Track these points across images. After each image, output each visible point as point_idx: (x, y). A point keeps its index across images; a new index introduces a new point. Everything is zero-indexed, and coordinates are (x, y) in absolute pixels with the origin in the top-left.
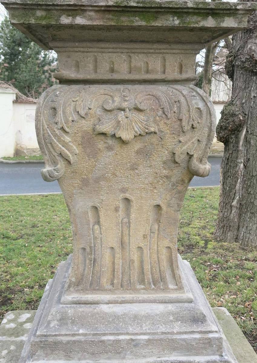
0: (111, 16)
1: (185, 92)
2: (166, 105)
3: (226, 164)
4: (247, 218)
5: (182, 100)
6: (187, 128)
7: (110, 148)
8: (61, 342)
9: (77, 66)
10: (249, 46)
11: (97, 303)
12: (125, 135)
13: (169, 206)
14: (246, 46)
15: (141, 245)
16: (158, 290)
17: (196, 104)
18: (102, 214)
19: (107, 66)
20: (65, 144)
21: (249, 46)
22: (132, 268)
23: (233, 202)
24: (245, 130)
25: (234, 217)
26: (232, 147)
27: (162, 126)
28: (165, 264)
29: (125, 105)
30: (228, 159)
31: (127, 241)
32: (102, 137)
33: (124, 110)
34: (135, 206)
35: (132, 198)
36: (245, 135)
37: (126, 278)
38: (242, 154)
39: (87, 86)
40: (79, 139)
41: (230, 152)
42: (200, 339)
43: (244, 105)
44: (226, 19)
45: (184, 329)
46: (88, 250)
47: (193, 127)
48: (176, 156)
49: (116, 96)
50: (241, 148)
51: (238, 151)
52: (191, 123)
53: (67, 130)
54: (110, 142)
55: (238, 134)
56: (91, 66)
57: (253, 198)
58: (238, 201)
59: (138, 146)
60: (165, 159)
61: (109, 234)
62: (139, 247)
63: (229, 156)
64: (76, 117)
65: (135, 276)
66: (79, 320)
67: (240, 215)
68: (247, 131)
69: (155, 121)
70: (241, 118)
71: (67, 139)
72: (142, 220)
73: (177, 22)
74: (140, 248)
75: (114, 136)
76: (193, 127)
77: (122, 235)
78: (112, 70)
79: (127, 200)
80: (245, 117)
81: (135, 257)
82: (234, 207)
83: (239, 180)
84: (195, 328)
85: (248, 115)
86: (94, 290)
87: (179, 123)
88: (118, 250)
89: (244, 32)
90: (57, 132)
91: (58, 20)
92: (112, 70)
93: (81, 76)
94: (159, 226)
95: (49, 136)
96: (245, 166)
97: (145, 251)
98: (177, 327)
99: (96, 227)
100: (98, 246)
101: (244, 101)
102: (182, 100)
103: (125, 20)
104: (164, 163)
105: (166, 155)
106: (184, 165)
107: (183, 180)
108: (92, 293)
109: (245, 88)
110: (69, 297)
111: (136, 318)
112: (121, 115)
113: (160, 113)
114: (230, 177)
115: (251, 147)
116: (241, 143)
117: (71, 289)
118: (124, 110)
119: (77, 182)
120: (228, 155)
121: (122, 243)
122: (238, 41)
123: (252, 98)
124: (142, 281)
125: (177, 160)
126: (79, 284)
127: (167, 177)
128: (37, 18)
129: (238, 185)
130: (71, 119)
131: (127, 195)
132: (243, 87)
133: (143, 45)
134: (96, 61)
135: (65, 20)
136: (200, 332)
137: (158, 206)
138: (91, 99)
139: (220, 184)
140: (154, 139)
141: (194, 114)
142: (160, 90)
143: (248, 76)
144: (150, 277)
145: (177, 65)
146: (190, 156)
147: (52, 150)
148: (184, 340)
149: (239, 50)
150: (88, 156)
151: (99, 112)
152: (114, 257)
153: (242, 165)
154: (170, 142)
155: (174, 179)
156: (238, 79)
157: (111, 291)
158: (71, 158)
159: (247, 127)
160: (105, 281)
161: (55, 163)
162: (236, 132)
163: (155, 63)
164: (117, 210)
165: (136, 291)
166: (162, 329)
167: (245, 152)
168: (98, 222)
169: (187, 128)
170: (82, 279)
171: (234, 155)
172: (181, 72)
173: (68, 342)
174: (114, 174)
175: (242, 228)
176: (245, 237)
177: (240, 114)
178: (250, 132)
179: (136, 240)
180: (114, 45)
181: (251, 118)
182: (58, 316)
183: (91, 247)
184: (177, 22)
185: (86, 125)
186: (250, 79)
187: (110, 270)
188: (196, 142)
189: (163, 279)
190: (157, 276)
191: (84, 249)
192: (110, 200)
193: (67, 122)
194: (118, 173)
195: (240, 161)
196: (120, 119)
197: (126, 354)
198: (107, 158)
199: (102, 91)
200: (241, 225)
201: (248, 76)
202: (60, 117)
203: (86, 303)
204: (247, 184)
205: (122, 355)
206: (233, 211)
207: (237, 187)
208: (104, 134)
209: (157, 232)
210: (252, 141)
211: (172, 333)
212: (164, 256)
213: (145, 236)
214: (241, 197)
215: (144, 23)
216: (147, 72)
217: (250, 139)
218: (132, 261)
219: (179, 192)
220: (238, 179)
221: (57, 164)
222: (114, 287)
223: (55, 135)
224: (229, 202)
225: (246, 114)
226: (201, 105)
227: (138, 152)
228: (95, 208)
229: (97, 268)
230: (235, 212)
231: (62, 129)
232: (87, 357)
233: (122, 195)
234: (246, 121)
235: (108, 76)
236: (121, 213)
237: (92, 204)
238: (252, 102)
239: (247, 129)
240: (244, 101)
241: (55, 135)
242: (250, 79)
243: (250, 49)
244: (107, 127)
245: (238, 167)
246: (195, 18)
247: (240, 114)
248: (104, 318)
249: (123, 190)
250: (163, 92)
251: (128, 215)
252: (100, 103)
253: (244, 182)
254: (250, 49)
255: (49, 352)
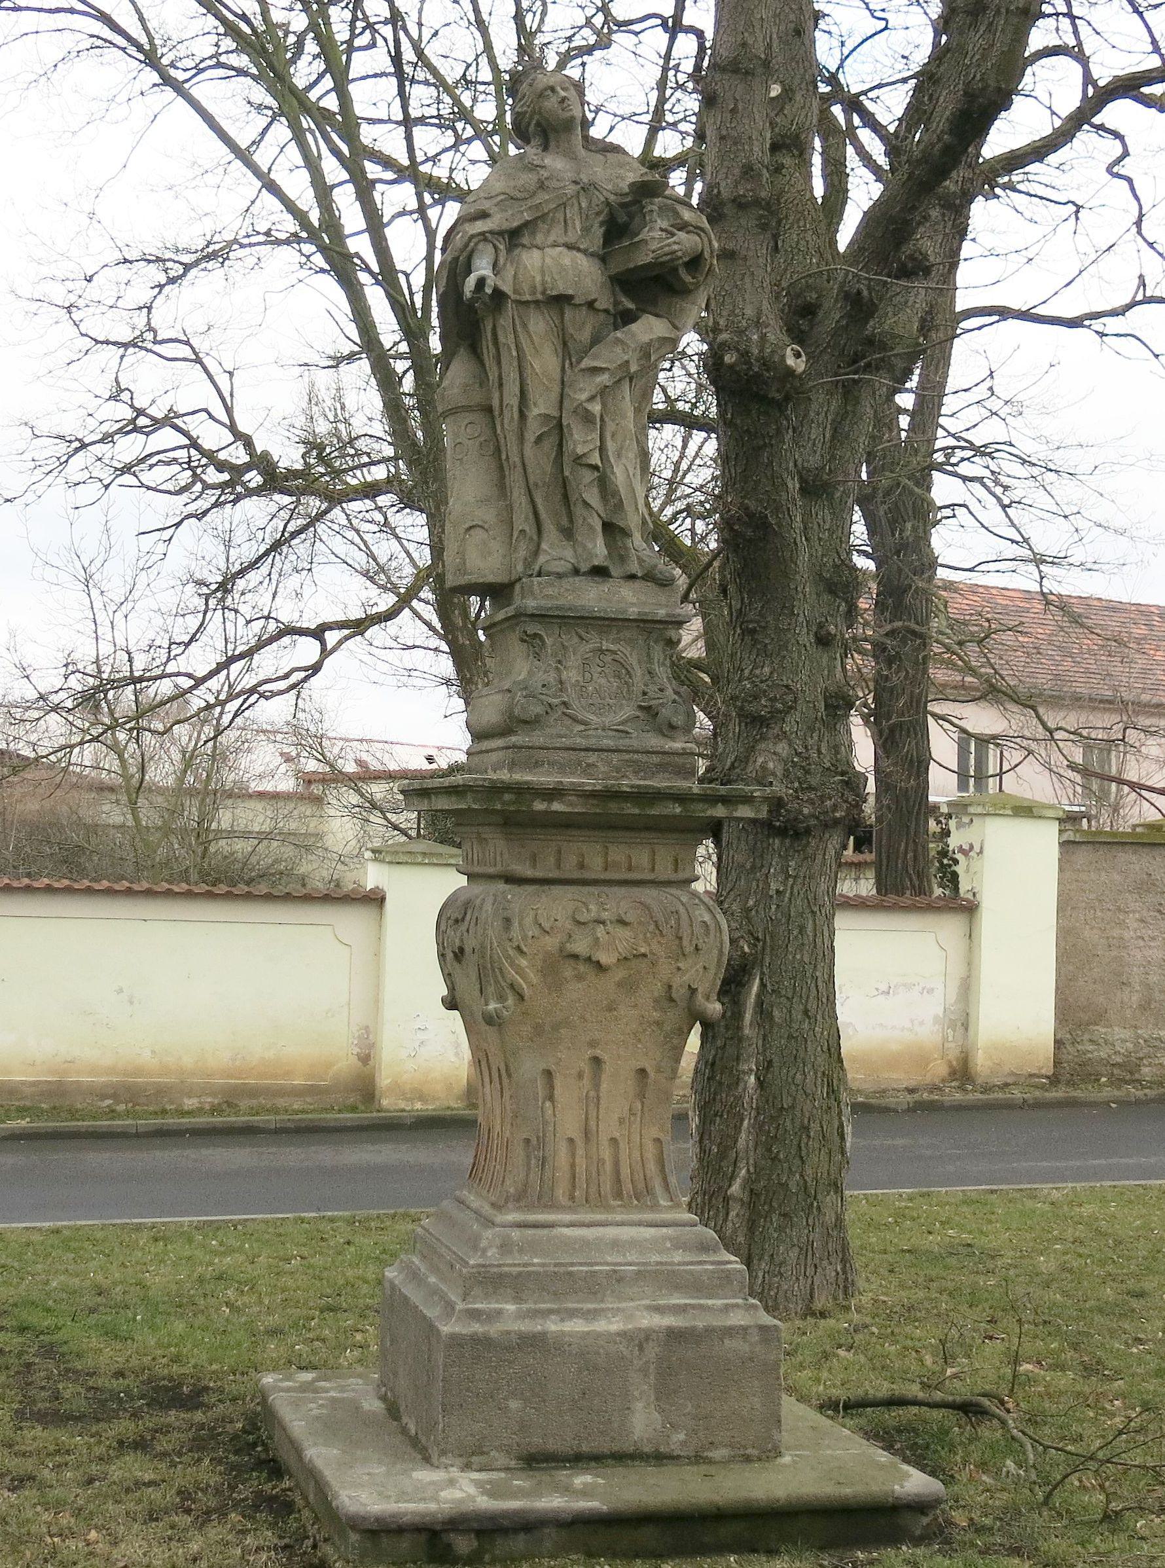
0: (595, 802)
1: (684, 899)
2: (660, 918)
3: (709, 1079)
4: (771, 1230)
5: (682, 910)
6: (689, 949)
7: (580, 978)
8: (508, 1275)
9: (534, 859)
10: (760, 760)
11: (551, 1226)
12: (605, 958)
13: (659, 1070)
14: (753, 759)
15: (617, 1135)
16: (642, 1208)
17: (700, 915)
18: (558, 1083)
19: (573, 860)
20: (520, 971)
21: (760, 760)
22: (602, 1173)
23: (730, 1186)
24: (757, 981)
25: (735, 1231)
26: (722, 1030)
27: (655, 947)
28: (652, 1167)
29: (605, 915)
30: (713, 1064)
31: (594, 1128)
32: (572, 962)
33: (603, 923)
34: (608, 1068)
35: (605, 1057)
36: (758, 996)
37: (593, 1190)
38: (751, 1049)
39: (546, 887)
40: (539, 963)
41: (719, 1043)
42: (713, 1272)
43: (753, 912)
44: (740, 806)
45: (688, 1259)
46: (534, 1141)
47: (697, 949)
48: (674, 991)
49: (593, 904)
50: (747, 1031)
51: (740, 1040)
52: (694, 943)
53: (525, 949)
54: (582, 968)
55: (739, 993)
56: (552, 860)
57: (786, 1171)
58: (747, 1181)
59: (619, 974)
60: (656, 994)
61: (568, 1120)
62: (612, 1139)
63: (715, 1057)
64: (537, 932)
65: (607, 1187)
66: (532, 1247)
67: (752, 1226)
68: (763, 985)
69: (646, 940)
70: (746, 949)
71: (524, 962)
72: (617, 1091)
73: (678, 810)
74: (614, 1141)
75: (589, 959)
76: (697, 949)
77: (587, 1119)
78: (581, 866)
79: (596, 1061)
80: (756, 946)
81: (606, 1153)
82: (735, 1199)
83: (746, 1122)
84: (704, 1258)
85: (765, 942)
86: (545, 1206)
87: (677, 942)
88: (580, 1143)
89: (746, 724)
90: (511, 952)
91: (530, 806)
92: (581, 866)
93: (539, 874)
94: (643, 1103)
95: (499, 957)
96: (761, 1083)
97: (621, 1145)
98: (678, 1256)
99: (548, 1104)
100: (550, 1135)
101: (751, 903)
102: (682, 910)
103: (613, 807)
104: (656, 1001)
105: (658, 989)
106: (684, 1004)
107: (680, 1029)
108: (542, 1212)
109: (753, 867)
110: (511, 1217)
111: (615, 1244)
112: (600, 931)
113: (652, 927)
114: (722, 1116)
115: (776, 1029)
116: (748, 1017)
117: (510, 1205)
118: (603, 923)
119: (526, 1029)
120: (713, 1052)
121: (587, 1133)
122: (731, 743)
123: (771, 897)
124: (618, 1195)
125: (674, 995)
126: (521, 1198)
127: (657, 1023)
128: (503, 804)
129: (743, 1135)
130: (530, 934)
131: (598, 1052)
132: (748, 866)
133: (628, 834)
134: (559, 852)
135: (539, 806)
136: (712, 1263)
137: (642, 1072)
138: (557, 907)
139: (691, 1142)
140: (643, 965)
141: (699, 930)
142: (649, 895)
143: (760, 836)
144: (630, 1186)
145: (671, 859)
146: (693, 991)
147: (500, 979)
148: (691, 1272)
149: (733, 767)
150: (549, 989)
151: (569, 925)
152: (573, 1155)
153: (752, 1078)
154: (665, 969)
155: (667, 1028)
156: (735, 842)
157: (570, 1210)
158: (527, 992)
159: (762, 973)
160: (561, 1194)
161: (501, 998)
162: (733, 986)
163: (641, 857)
164: (580, 1076)
165: (608, 1208)
166: (656, 1258)
167: (760, 1043)
168: (551, 1098)
169: (689, 949)
170: (525, 1191)
171: (731, 1051)
172: (676, 871)
173: (520, 1274)
174: (582, 1017)
175: (760, 1260)
176: (767, 1287)
177: (742, 937)
178: (769, 988)
179: (609, 1127)
180: (588, 833)
181: (773, 949)
182: (498, 1242)
183: (538, 1138)
184: (678, 810)
185: (551, 943)
186: (765, 845)
187: (568, 1176)
188: (701, 970)
189: (649, 1191)
190: (641, 1186)
191: (527, 1141)
192: (570, 1059)
193: (525, 938)
194: (588, 1016)
195: (746, 1068)
196: (599, 935)
197: (604, 1296)
198: (578, 991)
199: (570, 896)
200: (756, 1251)
201: (760, 836)
202: (515, 932)
203: (535, 1226)
204: (769, 1132)
205: (599, 1295)
206: (732, 1214)
207: (741, 1143)
208: (575, 957)
209: (639, 1113)
210: (776, 1013)
211: (672, 1264)
212: (650, 1151)
213: (621, 1121)
214: (752, 1170)
215: (637, 811)
216: (630, 869)
217: (772, 1006)
218: (600, 1162)
219: (675, 1048)
220: (742, 1120)
221: (506, 1000)
222: (573, 1204)
223: (508, 957)
224: (720, 1188)
225: (757, 939)
226: (707, 918)
227: (620, 984)
228: (548, 1074)
229: (548, 1174)
230: (737, 1215)
231: (519, 949)
232: (547, 1298)
233: (590, 1052)
234: (760, 957)
235: (576, 875)
236: (586, 1082)
237: (544, 1066)
238: (774, 907)
239: (761, 979)
240: (751, 903)
241: (508, 957)
242: (765, 845)
243: (764, 767)
244: (580, 946)
245: (742, 1085)
246: (700, 806)
247: (742, 937)
248: (568, 1245)
249: (593, 1044)
250: (653, 899)
251: (597, 1086)
252: (570, 912)
253: (759, 1127)
254: (764, 767)
255: (491, 1290)
